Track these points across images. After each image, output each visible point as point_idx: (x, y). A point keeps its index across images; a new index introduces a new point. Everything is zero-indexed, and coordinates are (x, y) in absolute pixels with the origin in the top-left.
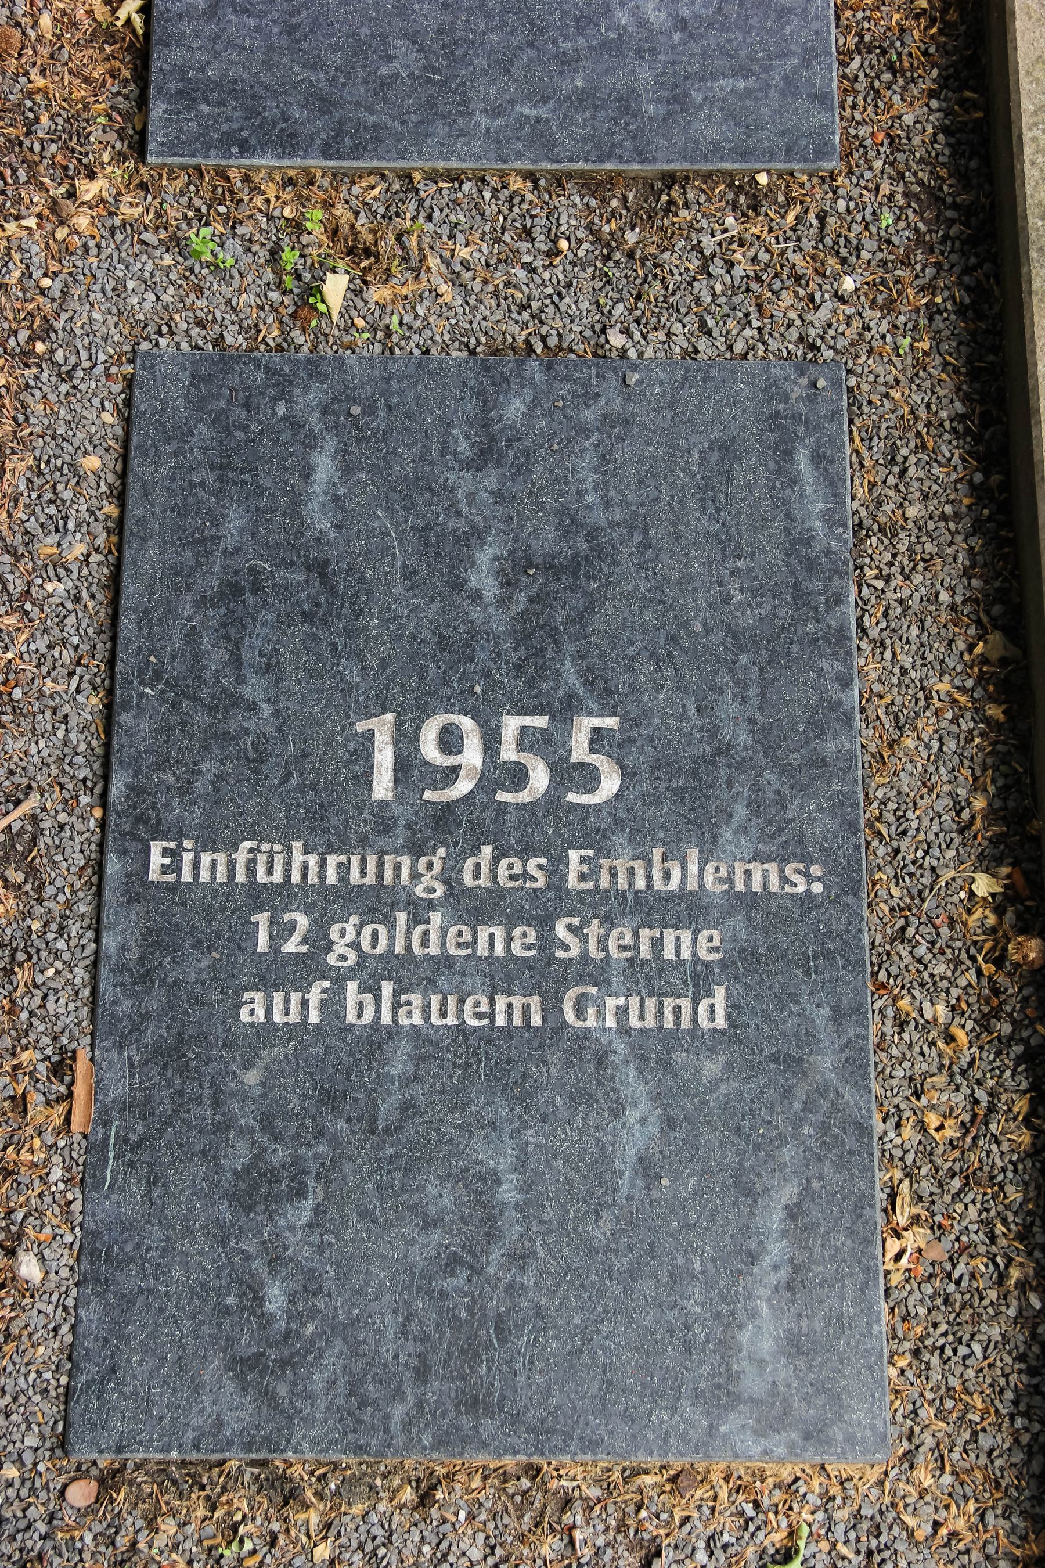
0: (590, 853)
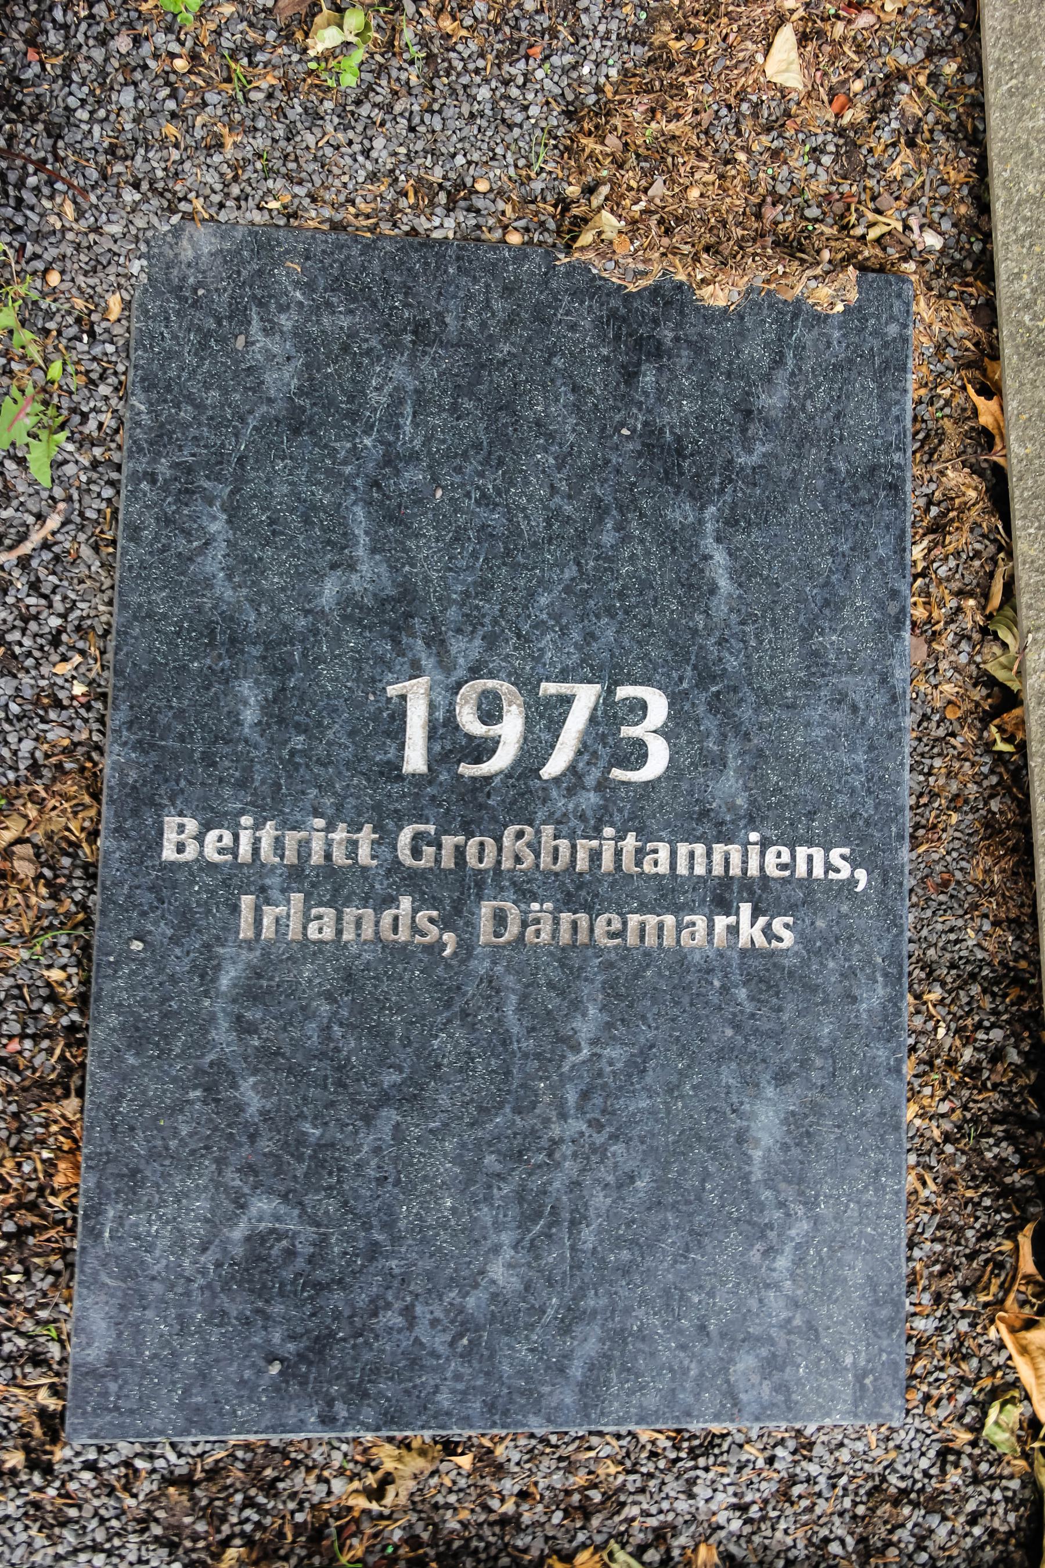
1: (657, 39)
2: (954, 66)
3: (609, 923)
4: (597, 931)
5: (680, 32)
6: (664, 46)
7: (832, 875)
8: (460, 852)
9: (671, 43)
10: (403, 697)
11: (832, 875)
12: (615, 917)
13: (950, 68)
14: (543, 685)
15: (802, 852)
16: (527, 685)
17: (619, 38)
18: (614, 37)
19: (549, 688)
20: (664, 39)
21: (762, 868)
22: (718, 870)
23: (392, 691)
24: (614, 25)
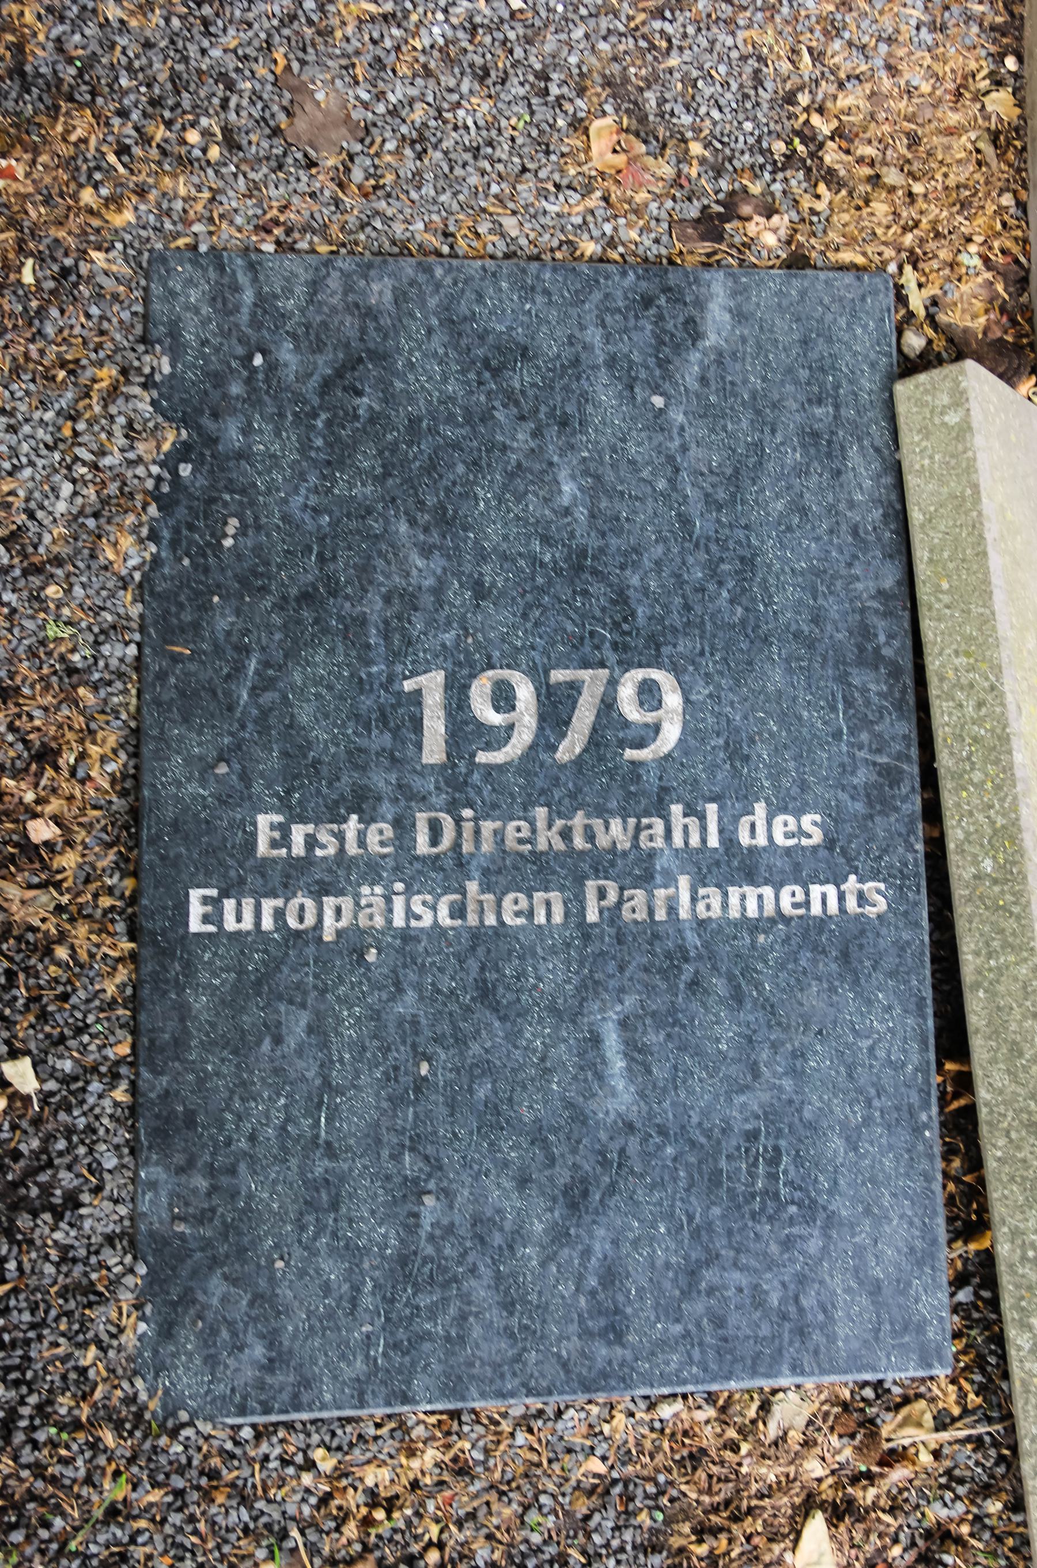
0: (213, 892)
1: (676, 1542)
2: (999, 1506)
3: (516, 902)
4: (719, 898)
5: (701, 1532)
6: (682, 1550)
7: (414, 923)
8: (499, 835)
9: (692, 1547)
10: (418, 692)
11: (414, 923)
12: (798, 889)
13: (994, 1507)
14: (553, 673)
15: (816, 890)
16: (538, 674)
17: (634, 1547)
18: (629, 1548)
19: (558, 676)
20: (683, 1542)
21: (725, 895)
22: (248, 904)
23: (408, 685)
24: (628, 1536)
